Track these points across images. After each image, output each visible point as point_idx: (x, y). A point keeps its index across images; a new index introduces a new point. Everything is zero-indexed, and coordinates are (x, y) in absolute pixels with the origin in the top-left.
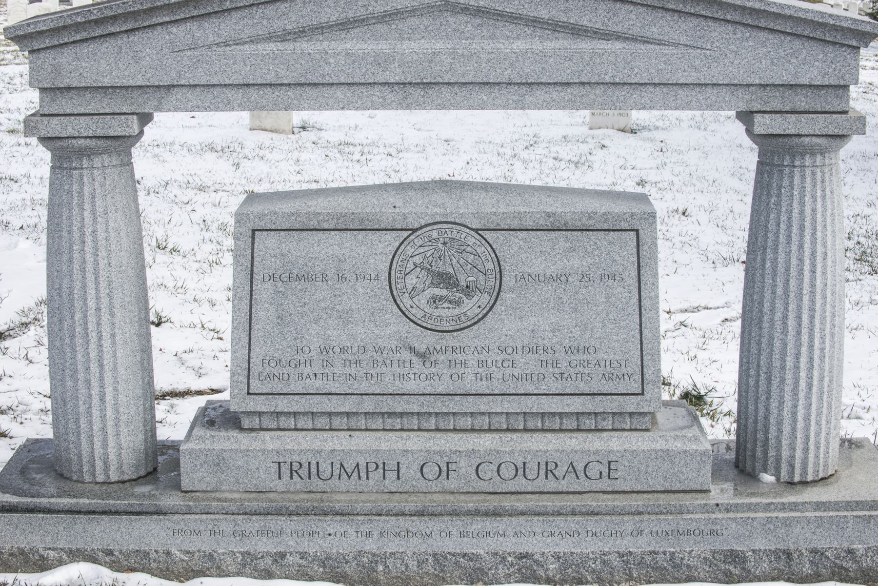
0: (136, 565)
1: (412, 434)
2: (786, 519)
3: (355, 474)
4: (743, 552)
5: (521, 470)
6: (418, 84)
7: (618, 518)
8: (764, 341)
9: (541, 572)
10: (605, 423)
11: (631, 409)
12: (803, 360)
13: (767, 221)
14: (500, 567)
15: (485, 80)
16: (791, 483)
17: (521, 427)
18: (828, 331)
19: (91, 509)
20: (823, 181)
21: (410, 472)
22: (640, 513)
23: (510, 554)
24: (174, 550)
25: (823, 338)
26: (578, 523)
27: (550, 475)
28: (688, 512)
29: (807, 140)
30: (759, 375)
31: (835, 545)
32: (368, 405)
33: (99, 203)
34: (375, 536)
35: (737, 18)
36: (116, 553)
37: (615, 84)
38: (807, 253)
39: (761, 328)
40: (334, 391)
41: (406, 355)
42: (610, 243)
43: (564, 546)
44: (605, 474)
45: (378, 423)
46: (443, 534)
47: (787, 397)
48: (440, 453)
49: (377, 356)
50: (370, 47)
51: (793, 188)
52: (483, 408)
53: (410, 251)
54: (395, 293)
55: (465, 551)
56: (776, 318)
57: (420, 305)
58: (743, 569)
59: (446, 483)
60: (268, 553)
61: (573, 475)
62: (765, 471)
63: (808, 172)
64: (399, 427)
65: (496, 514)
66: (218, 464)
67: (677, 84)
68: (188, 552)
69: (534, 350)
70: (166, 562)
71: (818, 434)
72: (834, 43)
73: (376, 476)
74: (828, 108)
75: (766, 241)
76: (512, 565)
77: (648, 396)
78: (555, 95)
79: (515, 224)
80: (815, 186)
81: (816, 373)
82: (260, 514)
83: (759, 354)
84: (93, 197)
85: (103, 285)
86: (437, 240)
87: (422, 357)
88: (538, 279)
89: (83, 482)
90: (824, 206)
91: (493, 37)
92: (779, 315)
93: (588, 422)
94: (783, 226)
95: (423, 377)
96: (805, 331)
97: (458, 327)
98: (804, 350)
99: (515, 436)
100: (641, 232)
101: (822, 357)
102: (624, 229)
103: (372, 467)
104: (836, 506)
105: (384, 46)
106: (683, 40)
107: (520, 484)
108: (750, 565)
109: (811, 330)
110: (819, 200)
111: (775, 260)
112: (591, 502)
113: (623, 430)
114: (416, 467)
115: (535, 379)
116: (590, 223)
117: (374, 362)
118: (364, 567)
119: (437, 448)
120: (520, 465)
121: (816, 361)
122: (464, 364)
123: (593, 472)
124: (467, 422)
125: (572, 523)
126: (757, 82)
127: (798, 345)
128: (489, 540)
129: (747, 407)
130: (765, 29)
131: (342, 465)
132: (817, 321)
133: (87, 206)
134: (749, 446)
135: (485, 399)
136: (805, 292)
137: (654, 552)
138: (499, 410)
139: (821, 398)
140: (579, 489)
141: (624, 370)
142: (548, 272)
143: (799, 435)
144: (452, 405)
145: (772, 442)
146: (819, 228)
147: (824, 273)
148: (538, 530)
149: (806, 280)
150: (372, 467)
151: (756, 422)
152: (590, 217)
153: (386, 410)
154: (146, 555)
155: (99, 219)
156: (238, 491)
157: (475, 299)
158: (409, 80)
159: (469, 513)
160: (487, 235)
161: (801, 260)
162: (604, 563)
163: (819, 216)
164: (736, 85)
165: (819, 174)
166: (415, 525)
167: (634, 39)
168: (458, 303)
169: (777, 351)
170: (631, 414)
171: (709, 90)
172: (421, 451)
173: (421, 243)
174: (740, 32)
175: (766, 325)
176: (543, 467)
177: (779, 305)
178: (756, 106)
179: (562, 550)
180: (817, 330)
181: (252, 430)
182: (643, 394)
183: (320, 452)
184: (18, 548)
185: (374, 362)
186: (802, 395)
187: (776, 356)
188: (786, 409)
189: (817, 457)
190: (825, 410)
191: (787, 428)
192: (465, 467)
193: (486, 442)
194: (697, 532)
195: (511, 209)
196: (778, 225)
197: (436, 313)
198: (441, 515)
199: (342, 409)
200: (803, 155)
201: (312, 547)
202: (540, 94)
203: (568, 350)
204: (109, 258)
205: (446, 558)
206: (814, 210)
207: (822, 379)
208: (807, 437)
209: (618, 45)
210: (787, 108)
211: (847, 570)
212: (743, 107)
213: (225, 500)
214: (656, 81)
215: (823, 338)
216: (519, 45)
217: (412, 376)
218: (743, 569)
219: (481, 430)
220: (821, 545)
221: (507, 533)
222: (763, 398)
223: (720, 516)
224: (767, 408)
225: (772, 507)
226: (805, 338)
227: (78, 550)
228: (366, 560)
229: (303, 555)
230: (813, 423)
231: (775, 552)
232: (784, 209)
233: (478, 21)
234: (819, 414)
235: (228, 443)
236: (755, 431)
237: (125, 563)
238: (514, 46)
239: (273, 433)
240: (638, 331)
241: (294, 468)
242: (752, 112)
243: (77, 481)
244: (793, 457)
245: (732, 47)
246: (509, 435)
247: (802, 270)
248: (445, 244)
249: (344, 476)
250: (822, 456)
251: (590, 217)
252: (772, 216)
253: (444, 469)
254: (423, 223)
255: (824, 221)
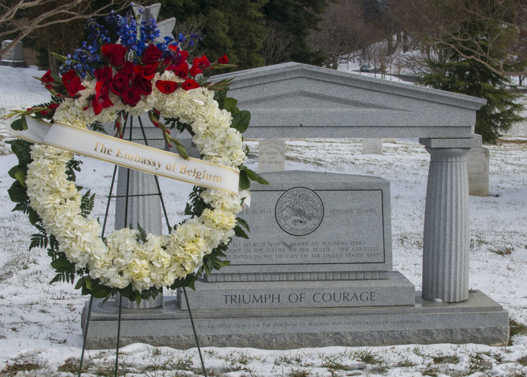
0: (163, 343)
1: (285, 282)
2: (449, 315)
3: (260, 300)
4: (431, 330)
5: (333, 297)
6: (289, 127)
7: (377, 316)
8: (436, 239)
9: (344, 341)
10: (368, 276)
11: (380, 269)
12: (453, 247)
13: (436, 186)
14: (326, 339)
15: (318, 125)
16: (449, 303)
17: (332, 279)
18: (463, 234)
19: (143, 318)
20: (460, 168)
21: (284, 299)
22: (386, 314)
23: (330, 333)
24: (181, 335)
25: (461, 237)
26: (360, 318)
27: (345, 299)
28: (407, 313)
29: (454, 150)
30: (433, 254)
31: (471, 326)
32: (265, 269)
33: (145, 179)
34: (272, 326)
35: (424, 98)
36: (155, 338)
37: (372, 127)
38: (454, 199)
39: (434, 234)
40: (250, 263)
41: (282, 246)
42: (370, 196)
43: (354, 329)
44: (369, 298)
45: (269, 278)
46: (302, 324)
47: (447, 263)
48: (298, 290)
49: (270, 247)
50: (268, 110)
51: (447, 171)
52: (315, 270)
53: (284, 200)
54: (278, 219)
55: (311, 332)
56: (441, 229)
57: (288, 224)
58: (432, 338)
59: (300, 303)
60: (224, 335)
61: (355, 299)
62: (438, 297)
63: (454, 164)
64: (278, 279)
65: (323, 315)
66: (199, 297)
67: (398, 127)
68: (188, 336)
69: (337, 243)
70: (178, 341)
71: (460, 280)
72: (465, 108)
73: (269, 301)
74: (463, 136)
75: (436, 195)
76: (331, 338)
77: (387, 263)
78: (347, 131)
79: (330, 188)
80: (457, 170)
81: (459, 253)
82: (220, 318)
83: (434, 245)
84: (143, 177)
85: (147, 217)
86: (296, 195)
87: (290, 247)
88: (339, 212)
89: (133, 309)
90: (461, 179)
91: (320, 106)
92: (442, 227)
93: (360, 276)
94: (443, 188)
95: (289, 256)
96: (454, 234)
97: (305, 234)
98: (454, 242)
99: (329, 282)
100: (383, 191)
101: (461, 245)
102: (375, 191)
103: (268, 297)
104: (471, 309)
105: (274, 110)
106: (401, 107)
107: (333, 303)
108: (435, 336)
109: (456, 233)
110: (459, 176)
111: (440, 203)
112: (366, 310)
113: (376, 279)
114: (287, 296)
115: (338, 256)
116: (362, 187)
117: (268, 250)
118: (267, 340)
119: (297, 288)
120: (332, 295)
121: (459, 247)
122: (307, 250)
123: (364, 297)
124: (308, 277)
125: (358, 318)
126: (432, 125)
127: (451, 240)
128: (321, 327)
129: (428, 270)
130: (436, 102)
131: (254, 296)
132: (459, 229)
133: (140, 181)
134: (429, 287)
135: (316, 266)
136: (453, 216)
137: (393, 331)
138: (322, 271)
139: (461, 264)
140: (358, 305)
141: (376, 252)
142: (344, 209)
143: (452, 281)
144: (302, 269)
145: (440, 284)
146: (459, 189)
147: (461, 208)
148: (343, 322)
149: (454, 211)
150: (268, 297)
151: (433, 276)
152: (362, 184)
153: (273, 271)
154: (169, 338)
155: (146, 187)
156: (207, 309)
157: (312, 221)
158: (285, 125)
159: (312, 315)
160: (317, 192)
161: (451, 203)
162: (371, 336)
163: (459, 183)
164: (423, 127)
165: (458, 165)
166: (289, 320)
167: (380, 107)
168: (305, 223)
169: (441, 243)
170: (379, 272)
171: (412, 129)
172: (289, 289)
173: (289, 196)
174: (425, 104)
175: (436, 232)
176: (342, 295)
177: (442, 222)
178: (432, 136)
179: (353, 331)
180: (459, 233)
181: (212, 282)
182: (384, 262)
183: (244, 290)
184: (108, 337)
185: (268, 250)
186: (453, 262)
187: (441, 245)
188: (446, 269)
189: (460, 291)
190: (463, 269)
191: (447, 277)
192: (308, 296)
193: (317, 285)
194: (411, 321)
195: (328, 181)
196: (441, 188)
197: (296, 227)
198: (300, 316)
199: (253, 272)
200: (451, 157)
201: (244, 332)
202: (340, 131)
203: (352, 243)
204: (149, 204)
205: (303, 335)
206: (457, 181)
207: (461, 256)
208: (456, 282)
209: (374, 110)
210: (445, 137)
211: (477, 338)
212: (425, 136)
213: (203, 312)
214: (390, 125)
215: (461, 237)
216: (332, 110)
217: (285, 256)
218: (432, 338)
219: (314, 280)
220: (465, 327)
221: (329, 323)
222: (436, 265)
223: (421, 314)
224: (438, 269)
225: (443, 310)
226: (454, 237)
227: (137, 337)
228: (267, 337)
229: (240, 336)
230: (458, 275)
231: (446, 330)
232: (444, 181)
233: (314, 100)
234: (460, 271)
235: (203, 288)
236: (432, 280)
237: (158, 342)
238: (330, 110)
239: (222, 283)
240: (382, 234)
241: (233, 298)
242: (430, 139)
243: (130, 309)
244: (449, 291)
245: (422, 110)
246: (327, 282)
247: (452, 207)
248: (299, 197)
249: (255, 301)
250: (462, 290)
251: (362, 184)
252: (438, 184)
253: (299, 297)
254: (290, 187)
255: (461, 185)
